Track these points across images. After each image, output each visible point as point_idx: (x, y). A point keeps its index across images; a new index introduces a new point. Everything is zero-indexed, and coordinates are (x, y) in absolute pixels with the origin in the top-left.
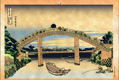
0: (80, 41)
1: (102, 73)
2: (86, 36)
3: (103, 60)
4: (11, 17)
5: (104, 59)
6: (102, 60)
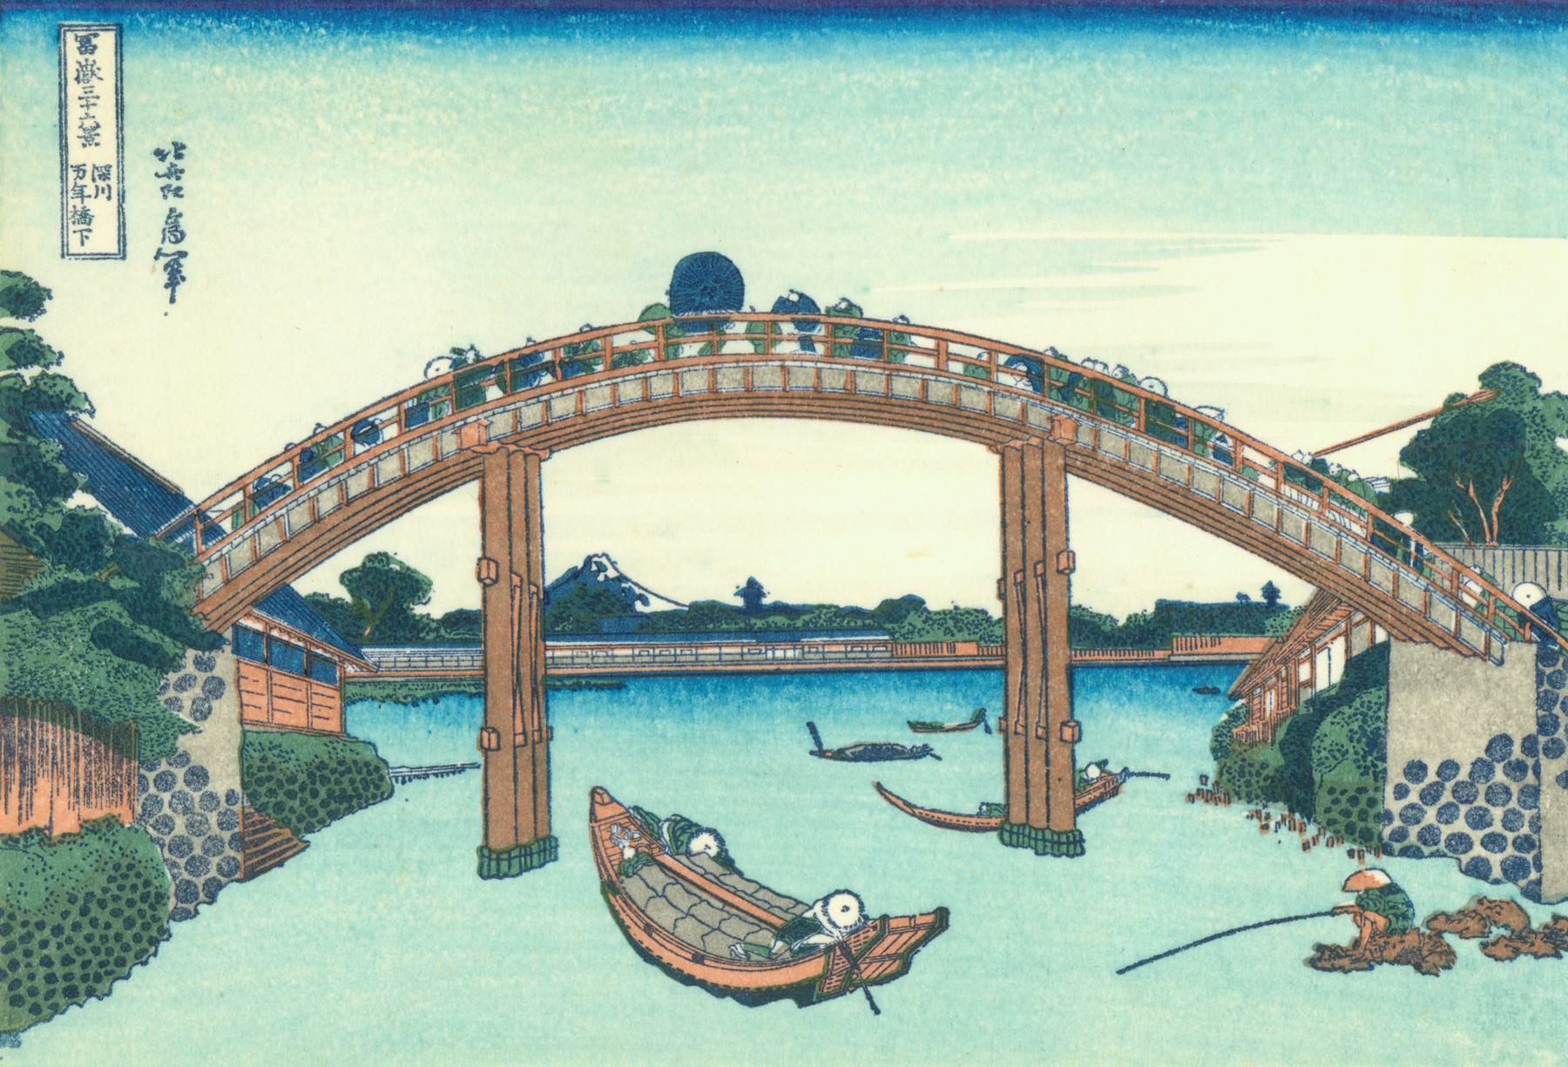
0: (1084, 497)
4: (104, 153)
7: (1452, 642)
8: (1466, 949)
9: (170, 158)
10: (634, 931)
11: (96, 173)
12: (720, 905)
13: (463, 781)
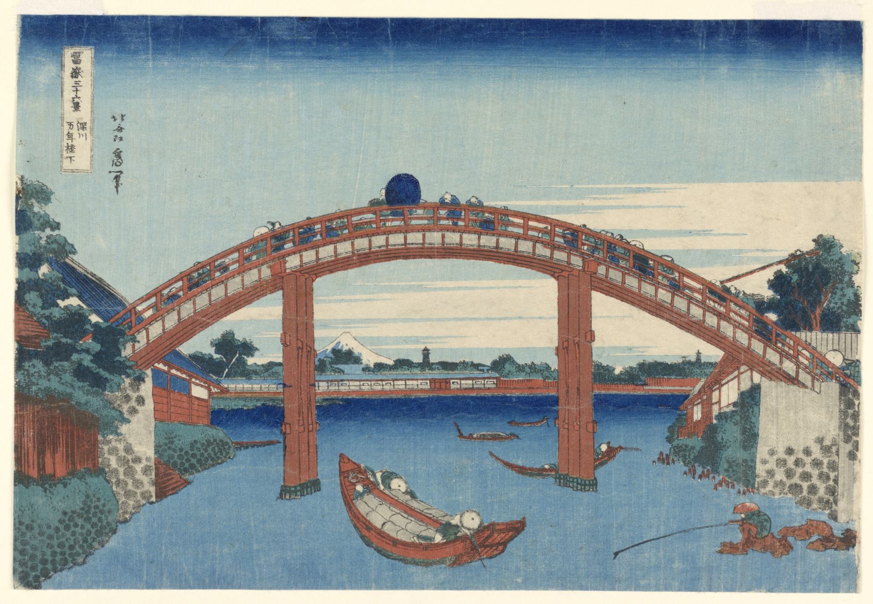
0: (598, 300)
7: (793, 380)
8: (799, 545)
9: (119, 121)
11: (79, 127)
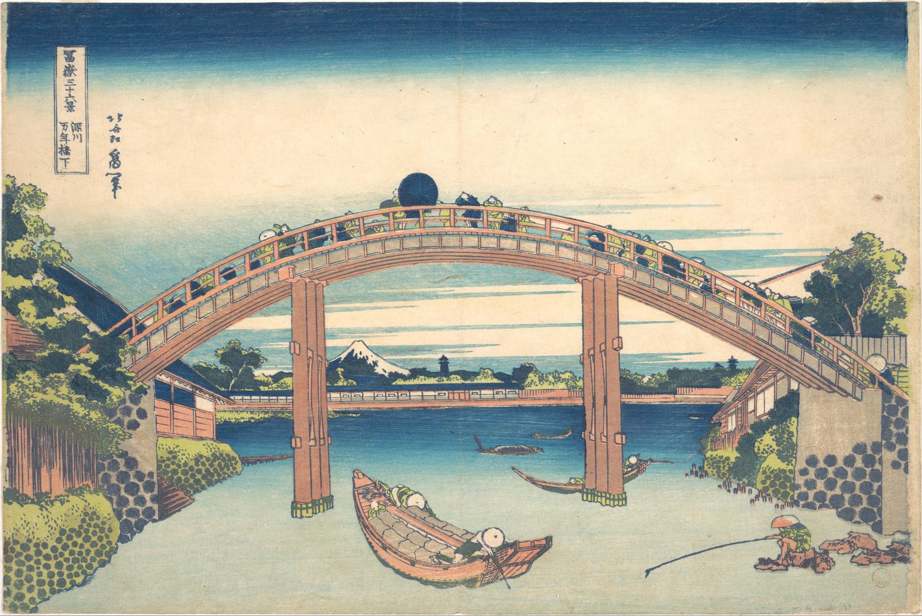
1: (805, 565)
2: (674, 274)
3: (142, 414)
4: (77, 116)
5: (821, 458)
6: (802, 464)
7: (832, 387)
9: (116, 120)
10: (377, 548)
12: (425, 534)
13: (334, 488)
